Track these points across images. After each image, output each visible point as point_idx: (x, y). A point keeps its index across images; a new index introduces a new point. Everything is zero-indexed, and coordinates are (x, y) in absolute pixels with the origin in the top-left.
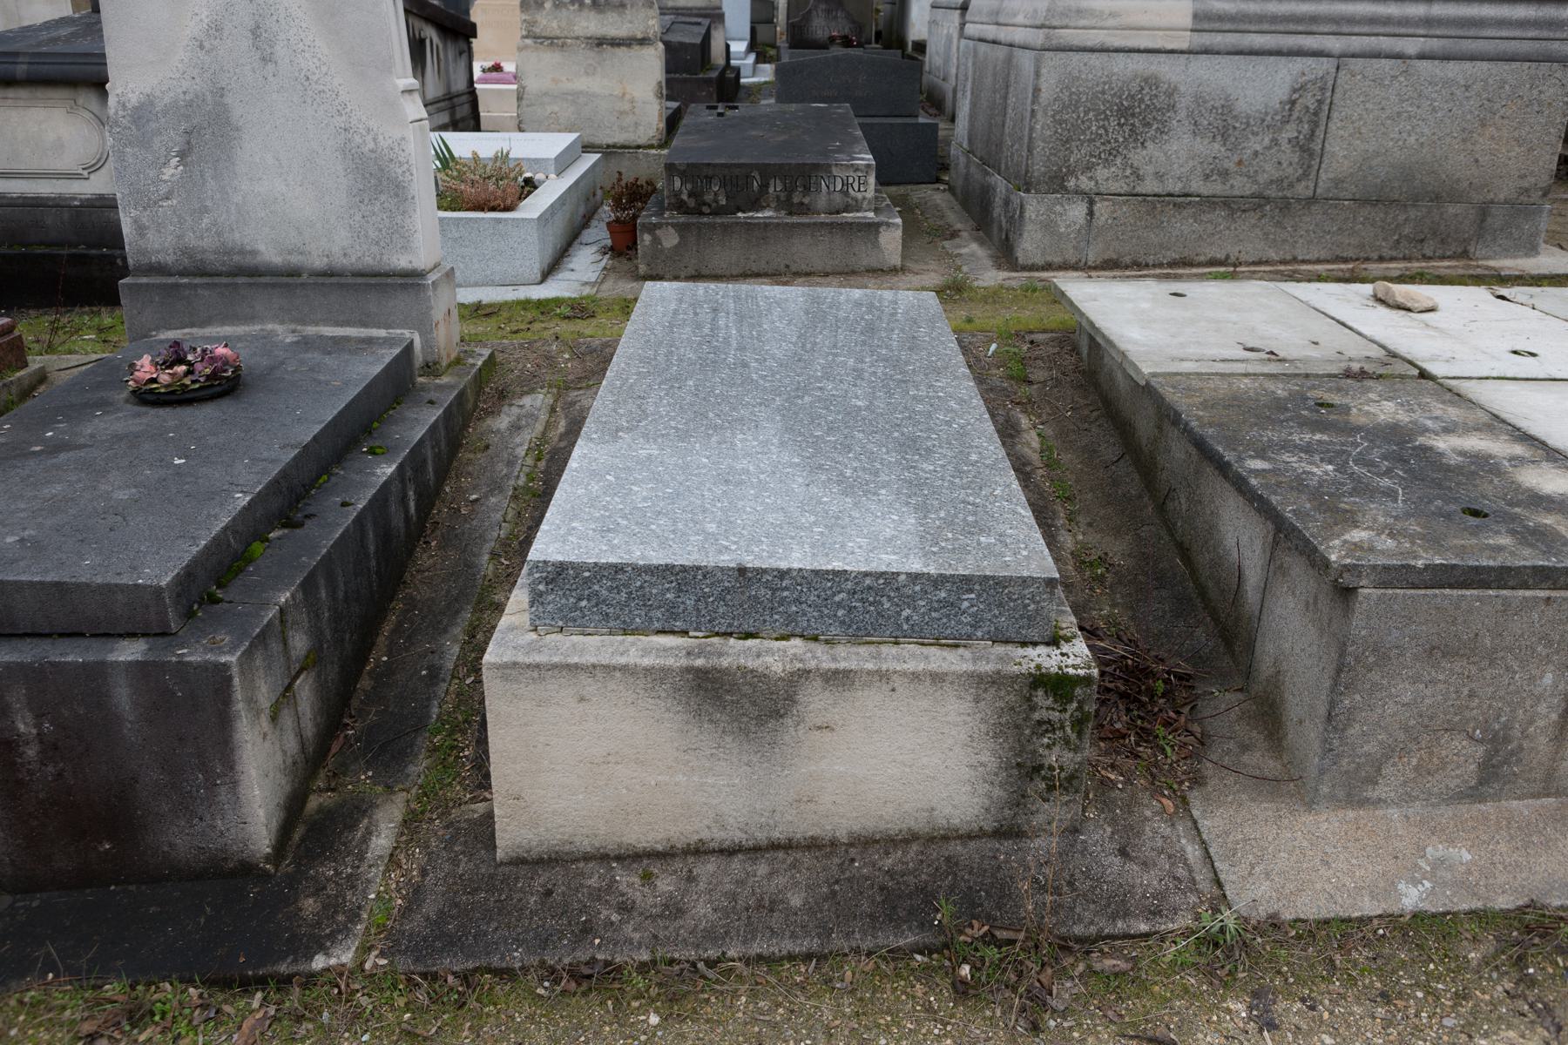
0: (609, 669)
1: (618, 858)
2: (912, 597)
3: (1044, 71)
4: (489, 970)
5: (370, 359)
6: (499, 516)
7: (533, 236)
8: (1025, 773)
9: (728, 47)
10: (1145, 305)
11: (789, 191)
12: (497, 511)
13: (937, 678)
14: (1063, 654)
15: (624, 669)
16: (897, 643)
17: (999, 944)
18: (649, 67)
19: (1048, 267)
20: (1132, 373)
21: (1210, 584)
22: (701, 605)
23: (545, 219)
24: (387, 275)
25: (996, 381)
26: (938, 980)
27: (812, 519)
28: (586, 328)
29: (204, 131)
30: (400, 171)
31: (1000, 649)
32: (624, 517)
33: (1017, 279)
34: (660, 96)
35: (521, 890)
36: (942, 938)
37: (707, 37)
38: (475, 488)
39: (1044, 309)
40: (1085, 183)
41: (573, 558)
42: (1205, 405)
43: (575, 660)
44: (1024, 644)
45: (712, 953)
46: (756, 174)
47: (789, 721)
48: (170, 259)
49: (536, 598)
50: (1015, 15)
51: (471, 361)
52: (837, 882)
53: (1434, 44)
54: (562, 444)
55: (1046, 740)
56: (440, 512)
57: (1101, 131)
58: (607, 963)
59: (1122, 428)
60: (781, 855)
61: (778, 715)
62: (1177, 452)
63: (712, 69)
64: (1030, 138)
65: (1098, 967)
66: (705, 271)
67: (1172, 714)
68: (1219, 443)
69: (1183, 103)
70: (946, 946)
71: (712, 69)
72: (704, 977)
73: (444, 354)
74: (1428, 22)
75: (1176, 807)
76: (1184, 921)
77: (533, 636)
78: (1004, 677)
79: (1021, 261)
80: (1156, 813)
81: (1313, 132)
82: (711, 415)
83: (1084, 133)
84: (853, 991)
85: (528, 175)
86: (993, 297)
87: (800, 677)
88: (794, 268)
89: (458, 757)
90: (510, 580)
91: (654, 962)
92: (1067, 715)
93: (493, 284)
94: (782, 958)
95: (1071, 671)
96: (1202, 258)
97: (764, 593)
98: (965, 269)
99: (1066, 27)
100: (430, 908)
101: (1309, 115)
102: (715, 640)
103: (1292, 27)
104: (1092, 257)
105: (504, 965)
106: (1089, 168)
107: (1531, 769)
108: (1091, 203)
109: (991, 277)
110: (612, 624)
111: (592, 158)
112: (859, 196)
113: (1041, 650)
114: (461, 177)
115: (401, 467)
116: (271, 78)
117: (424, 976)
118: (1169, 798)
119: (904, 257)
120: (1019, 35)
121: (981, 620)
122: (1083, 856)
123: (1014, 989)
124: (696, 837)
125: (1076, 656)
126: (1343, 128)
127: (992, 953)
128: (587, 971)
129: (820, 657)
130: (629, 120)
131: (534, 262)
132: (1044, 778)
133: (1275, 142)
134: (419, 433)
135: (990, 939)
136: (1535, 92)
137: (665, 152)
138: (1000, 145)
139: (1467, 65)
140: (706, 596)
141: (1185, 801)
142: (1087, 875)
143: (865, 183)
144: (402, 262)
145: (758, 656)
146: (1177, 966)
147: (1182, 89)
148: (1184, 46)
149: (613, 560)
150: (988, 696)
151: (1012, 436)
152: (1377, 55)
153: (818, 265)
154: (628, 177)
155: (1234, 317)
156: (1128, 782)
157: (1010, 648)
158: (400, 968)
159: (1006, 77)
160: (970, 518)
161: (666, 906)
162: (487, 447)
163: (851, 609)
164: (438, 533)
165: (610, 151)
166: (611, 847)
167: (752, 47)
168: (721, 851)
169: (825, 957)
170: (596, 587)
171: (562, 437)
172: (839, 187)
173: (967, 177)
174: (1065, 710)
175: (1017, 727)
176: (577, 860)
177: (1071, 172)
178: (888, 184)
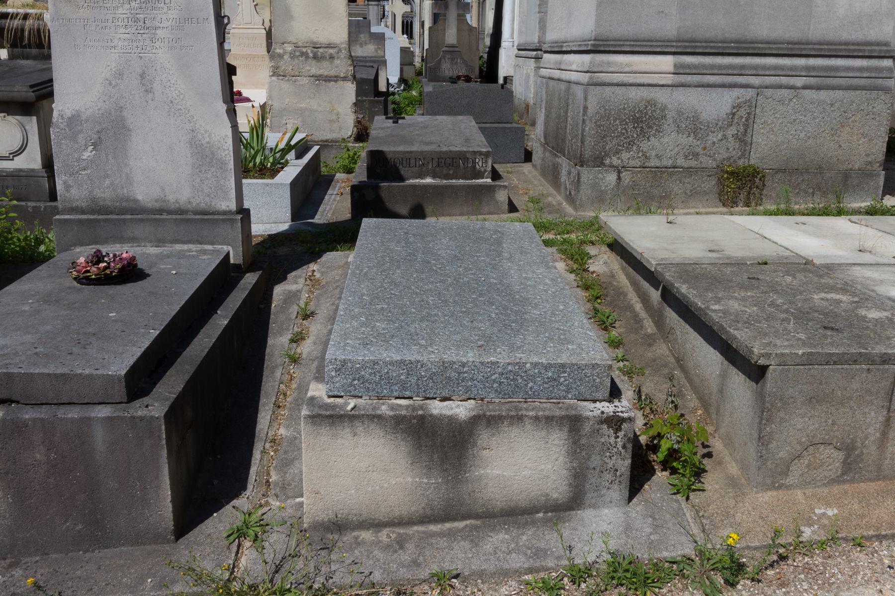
2: (534, 376)
3: (589, 97)
9: (388, 80)
16: (526, 402)
22: (420, 382)
24: (213, 213)
29: (111, 131)
32: (375, 337)
40: (616, 161)
44: (595, 401)
48: (84, 205)
50: (571, 65)
53: (812, 81)
57: (624, 131)
64: (583, 135)
69: (670, 115)
74: (808, 68)
81: (746, 130)
95: (620, 414)
97: (454, 375)
101: (743, 120)
103: (730, 72)
106: (617, 152)
107: (869, 465)
108: (619, 172)
116: (150, 102)
120: (574, 76)
126: (763, 128)
130: (335, 125)
133: (725, 137)
136: (870, 107)
138: (564, 140)
139: (831, 92)
140: (422, 377)
148: (670, 82)
152: (780, 87)
159: (566, 100)
170: (363, 373)
177: (607, 155)
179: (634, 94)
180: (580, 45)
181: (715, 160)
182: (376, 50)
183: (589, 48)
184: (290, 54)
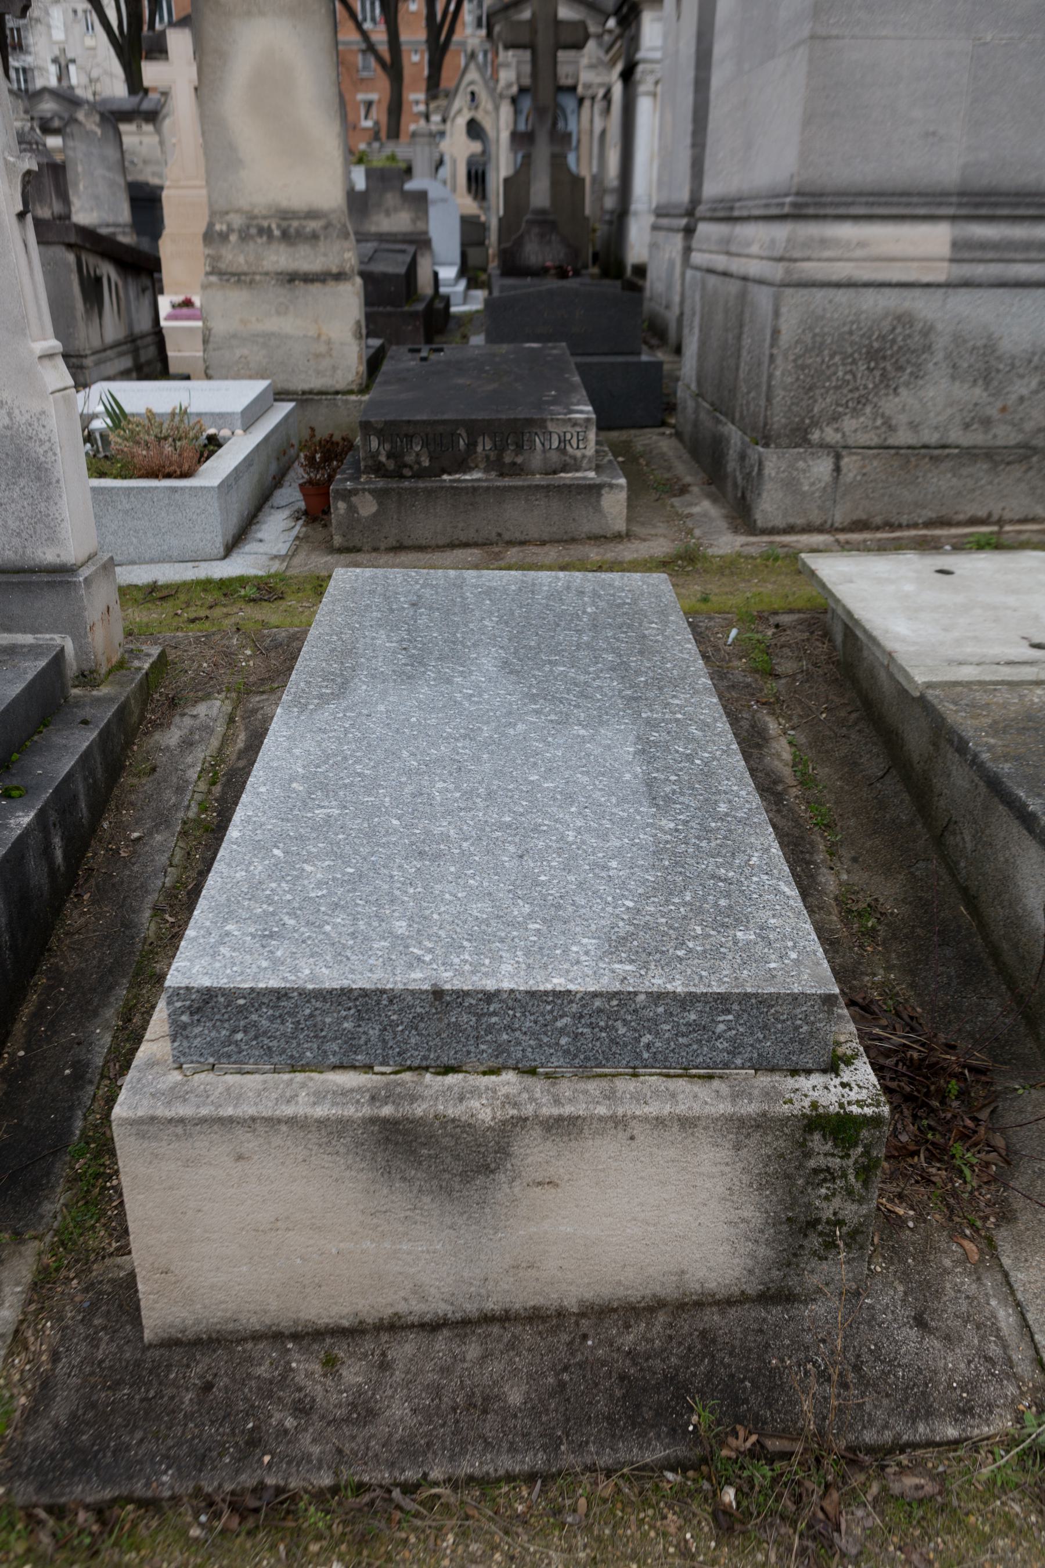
0: (272, 1122)
1: (295, 1337)
2: (655, 1021)
3: (784, 310)
4: (129, 1500)
5: (10, 675)
6: (164, 859)
7: (214, 507)
8: (800, 1231)
9: (436, 275)
10: (909, 588)
11: (500, 449)
12: (164, 848)
13: (687, 1123)
14: (844, 1085)
15: (291, 1121)
16: (635, 1075)
17: (771, 1459)
18: (347, 304)
19: (790, 530)
20: (902, 680)
21: (1005, 946)
23: (226, 486)
24: (32, 571)
25: (738, 676)
26: (694, 1507)
27: (527, 909)
28: (269, 614)
30: (41, 451)
31: (764, 1080)
32: (292, 914)
33: (756, 545)
34: (358, 336)
35: (174, 1383)
36: (698, 1451)
37: (413, 267)
38: (138, 821)
39: (787, 581)
40: (831, 436)
41: (223, 982)
42: (995, 729)
43: (229, 1111)
44: (794, 1072)
45: (411, 1475)
46: (462, 431)
47: (502, 1177)
49: (178, 1031)
50: (749, 244)
51: (136, 663)
52: (566, 1369)
54: (241, 764)
55: (823, 1191)
56: (97, 855)
57: (848, 377)
58: (279, 1490)
59: (890, 739)
60: (496, 1330)
61: (487, 1170)
62: (957, 782)
63: (419, 300)
65: (896, 1488)
66: (407, 542)
67: (969, 1123)
68: (1020, 785)
69: (941, 343)
70: (704, 1460)
71: (419, 300)
72: (399, 1507)
73: (102, 659)
75: (981, 1252)
76: (1003, 1423)
77: (176, 1076)
78: (771, 1119)
79: (760, 524)
80: (957, 1263)
82: (405, 754)
83: (829, 379)
84: (589, 1529)
85: (212, 431)
86: (729, 567)
87: (514, 1126)
88: (507, 537)
89: (104, 1188)
90: (157, 996)
91: (335, 1490)
92: (851, 1162)
93: (171, 560)
94: (498, 1480)
95: (855, 1109)
96: (961, 517)
98: (697, 532)
99: (808, 259)
100: (60, 1410)
102: (407, 1076)
104: (839, 517)
105: (149, 1494)
106: (835, 418)
108: (838, 457)
109: (727, 543)
110: (276, 1060)
111: (288, 406)
112: (578, 454)
113: (817, 1079)
114: (134, 438)
115: (41, 815)
117: (50, 1509)
118: (972, 1240)
119: (629, 520)
120: (754, 268)
121: (741, 1045)
122: (871, 1327)
123: (794, 1524)
124: (390, 1311)
125: (858, 1087)
127: (762, 1474)
128: (252, 1503)
129: (539, 1098)
130: (326, 363)
131: (216, 539)
132: (820, 1234)
134: (67, 764)
135: (757, 1453)
137: (366, 398)
140: (393, 1025)
141: (990, 1242)
142: (877, 1355)
143: (585, 439)
144: (49, 556)
145: (461, 1099)
146: (995, 1487)
147: (940, 327)
148: (942, 278)
149: (274, 983)
150: (752, 1142)
151: (759, 746)
153: (534, 533)
154: (322, 434)
155: (1012, 600)
156: (920, 1218)
157: (777, 1077)
158: (19, 1500)
159: (739, 314)
160: (723, 902)
161: (353, 1406)
162: (154, 769)
163: (576, 1036)
164: (93, 882)
165: (305, 398)
166: (285, 1325)
167: (463, 272)
168: (422, 1326)
169: (553, 1477)
170: (254, 1017)
171: (241, 754)
172: (555, 444)
173: (696, 424)
174: (848, 1156)
175: (788, 1176)
176: (245, 1340)
177: (815, 424)
178: (610, 428)
179: (415, 58)
180: (767, 206)
181: (1021, 430)
182: (414, 221)
183: (786, 210)
184: (240, 231)
